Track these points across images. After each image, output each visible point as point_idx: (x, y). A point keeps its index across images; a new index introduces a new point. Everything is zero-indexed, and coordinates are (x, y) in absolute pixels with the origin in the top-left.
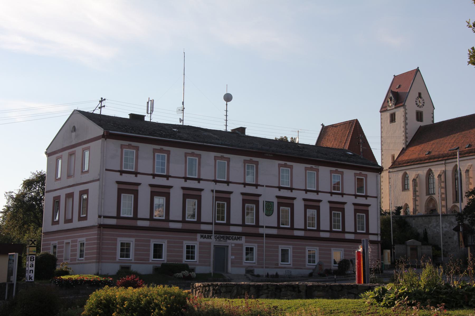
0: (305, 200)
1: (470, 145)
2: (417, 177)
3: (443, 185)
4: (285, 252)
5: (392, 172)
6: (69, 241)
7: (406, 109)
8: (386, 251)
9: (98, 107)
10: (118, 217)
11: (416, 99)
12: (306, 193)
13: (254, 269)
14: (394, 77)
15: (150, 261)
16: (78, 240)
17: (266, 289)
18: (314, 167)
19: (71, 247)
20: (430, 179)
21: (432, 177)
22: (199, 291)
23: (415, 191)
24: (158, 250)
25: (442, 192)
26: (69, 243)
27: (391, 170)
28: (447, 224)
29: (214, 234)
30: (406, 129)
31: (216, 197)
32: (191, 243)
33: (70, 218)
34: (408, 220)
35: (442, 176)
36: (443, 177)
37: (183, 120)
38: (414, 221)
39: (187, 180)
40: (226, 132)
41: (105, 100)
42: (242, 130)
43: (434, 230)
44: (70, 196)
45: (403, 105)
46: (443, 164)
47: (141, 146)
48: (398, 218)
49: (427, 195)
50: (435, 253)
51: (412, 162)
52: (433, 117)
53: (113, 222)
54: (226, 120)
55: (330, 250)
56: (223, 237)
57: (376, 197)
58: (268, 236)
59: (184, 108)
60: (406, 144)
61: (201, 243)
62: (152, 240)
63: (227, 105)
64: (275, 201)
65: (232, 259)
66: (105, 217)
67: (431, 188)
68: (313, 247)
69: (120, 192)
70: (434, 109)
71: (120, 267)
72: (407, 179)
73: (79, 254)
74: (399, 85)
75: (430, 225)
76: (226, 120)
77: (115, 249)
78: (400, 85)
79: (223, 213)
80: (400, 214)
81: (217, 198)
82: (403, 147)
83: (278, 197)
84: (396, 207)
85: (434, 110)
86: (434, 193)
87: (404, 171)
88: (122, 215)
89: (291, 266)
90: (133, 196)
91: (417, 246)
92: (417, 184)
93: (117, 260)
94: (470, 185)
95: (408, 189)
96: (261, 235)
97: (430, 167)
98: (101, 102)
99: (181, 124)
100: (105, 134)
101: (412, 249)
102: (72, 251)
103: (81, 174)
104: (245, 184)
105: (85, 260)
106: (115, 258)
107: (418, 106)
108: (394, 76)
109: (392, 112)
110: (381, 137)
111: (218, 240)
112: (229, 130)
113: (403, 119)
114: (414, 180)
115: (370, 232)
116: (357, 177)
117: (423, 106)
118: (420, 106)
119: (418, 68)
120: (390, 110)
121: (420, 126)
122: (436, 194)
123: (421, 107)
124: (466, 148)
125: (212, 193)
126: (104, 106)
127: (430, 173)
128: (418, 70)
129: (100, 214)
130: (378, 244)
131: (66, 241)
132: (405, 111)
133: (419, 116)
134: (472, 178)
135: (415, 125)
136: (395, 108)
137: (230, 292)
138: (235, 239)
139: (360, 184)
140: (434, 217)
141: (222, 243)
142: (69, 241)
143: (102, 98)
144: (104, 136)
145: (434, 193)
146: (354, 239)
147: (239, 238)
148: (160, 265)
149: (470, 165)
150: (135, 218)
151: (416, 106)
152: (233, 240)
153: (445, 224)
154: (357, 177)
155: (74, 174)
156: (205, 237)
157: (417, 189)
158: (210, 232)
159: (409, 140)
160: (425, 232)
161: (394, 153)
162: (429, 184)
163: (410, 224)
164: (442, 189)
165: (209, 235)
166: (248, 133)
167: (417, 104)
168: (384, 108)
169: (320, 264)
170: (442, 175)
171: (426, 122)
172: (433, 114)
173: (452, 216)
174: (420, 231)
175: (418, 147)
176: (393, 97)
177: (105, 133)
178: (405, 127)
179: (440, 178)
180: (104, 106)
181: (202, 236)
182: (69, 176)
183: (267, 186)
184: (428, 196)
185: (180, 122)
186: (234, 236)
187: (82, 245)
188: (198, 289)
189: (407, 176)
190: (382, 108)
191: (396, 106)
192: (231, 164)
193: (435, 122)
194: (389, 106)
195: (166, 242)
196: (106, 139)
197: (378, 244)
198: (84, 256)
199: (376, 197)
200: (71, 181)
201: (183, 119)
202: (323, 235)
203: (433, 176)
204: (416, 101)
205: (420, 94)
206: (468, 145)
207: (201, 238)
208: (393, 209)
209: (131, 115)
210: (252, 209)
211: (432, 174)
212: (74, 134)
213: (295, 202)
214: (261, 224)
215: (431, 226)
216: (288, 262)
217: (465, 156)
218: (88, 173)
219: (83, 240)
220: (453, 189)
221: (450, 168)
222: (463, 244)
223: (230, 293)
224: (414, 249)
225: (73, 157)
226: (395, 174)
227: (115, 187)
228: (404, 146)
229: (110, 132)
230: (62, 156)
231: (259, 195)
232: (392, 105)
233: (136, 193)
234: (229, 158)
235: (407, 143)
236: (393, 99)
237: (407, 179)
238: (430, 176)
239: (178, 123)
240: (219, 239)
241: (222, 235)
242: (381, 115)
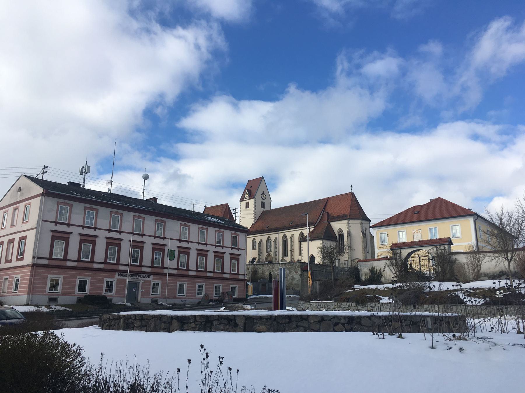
0: (197, 250)
4: (181, 287)
6: (7, 277)
9: (41, 172)
10: (50, 258)
12: (198, 245)
13: (158, 299)
15: (75, 294)
16: (15, 277)
17: (193, 322)
18: (205, 227)
19: (8, 282)
21: (270, 242)
22: (107, 324)
23: (260, 250)
24: (82, 286)
25: (276, 250)
26: (7, 279)
29: (129, 273)
30: (255, 212)
31: (132, 245)
32: (110, 280)
33: (10, 258)
37: (111, 190)
39: (111, 232)
40: (143, 200)
41: (47, 167)
42: (155, 199)
44: (11, 241)
47: (75, 204)
49: (266, 252)
52: (270, 206)
53: (46, 262)
54: (144, 193)
56: (136, 276)
57: (245, 250)
58: (171, 275)
59: (112, 182)
61: (118, 280)
62: (78, 277)
63: (144, 182)
64: (177, 250)
65: (142, 292)
66: (38, 258)
68: (201, 283)
69: (53, 238)
71: (48, 298)
73: (14, 288)
76: (144, 193)
77: (46, 284)
79: (137, 257)
81: (133, 247)
83: (178, 247)
85: (271, 202)
87: (254, 238)
88: (54, 257)
89: (185, 297)
90: (64, 242)
93: (47, 293)
95: (256, 249)
96: (165, 274)
97: (270, 236)
98: (44, 169)
99: (110, 192)
100: (44, 193)
102: (9, 285)
103: (22, 224)
104: (155, 237)
105: (18, 293)
106: (45, 291)
107: (262, 199)
111: (132, 277)
112: (145, 199)
113: (253, 206)
115: (240, 273)
116: (233, 235)
125: (130, 242)
126: (46, 172)
127: (269, 239)
129: (34, 256)
130: (244, 281)
131: (5, 277)
133: (263, 205)
135: (260, 210)
136: (249, 199)
137: (146, 326)
138: (145, 277)
139: (234, 240)
140: (276, 265)
141: (135, 280)
142: (7, 277)
143: (45, 166)
144: (42, 194)
147: (148, 276)
148: (83, 297)
150: (65, 259)
152: (143, 277)
154: (233, 235)
155: (16, 224)
156: (122, 275)
158: (126, 271)
165: (125, 273)
166: (158, 202)
167: (262, 198)
169: (206, 295)
171: (267, 208)
172: (271, 204)
177: (44, 191)
180: (46, 172)
181: (119, 275)
182: (12, 225)
183: (171, 239)
185: (109, 191)
186: (145, 275)
187: (17, 280)
188: (106, 321)
189: (255, 241)
192: (146, 222)
193: (272, 209)
195: (90, 279)
196: (45, 197)
198: (18, 290)
199: (245, 250)
200: (14, 230)
201: (111, 189)
202: (209, 275)
204: (261, 196)
205: (263, 192)
207: (118, 276)
209: (70, 183)
210: (159, 255)
212: (19, 193)
213: (191, 251)
214: (165, 266)
216: (183, 294)
218: (28, 223)
219: (18, 276)
221: (281, 235)
222: (311, 279)
223: (145, 328)
225: (17, 211)
227: (49, 235)
229: (49, 191)
230: (8, 210)
231: (165, 245)
233: (67, 240)
234: (145, 217)
235: (256, 221)
239: (107, 191)
240: (133, 277)
241: (135, 274)
242: (240, 203)
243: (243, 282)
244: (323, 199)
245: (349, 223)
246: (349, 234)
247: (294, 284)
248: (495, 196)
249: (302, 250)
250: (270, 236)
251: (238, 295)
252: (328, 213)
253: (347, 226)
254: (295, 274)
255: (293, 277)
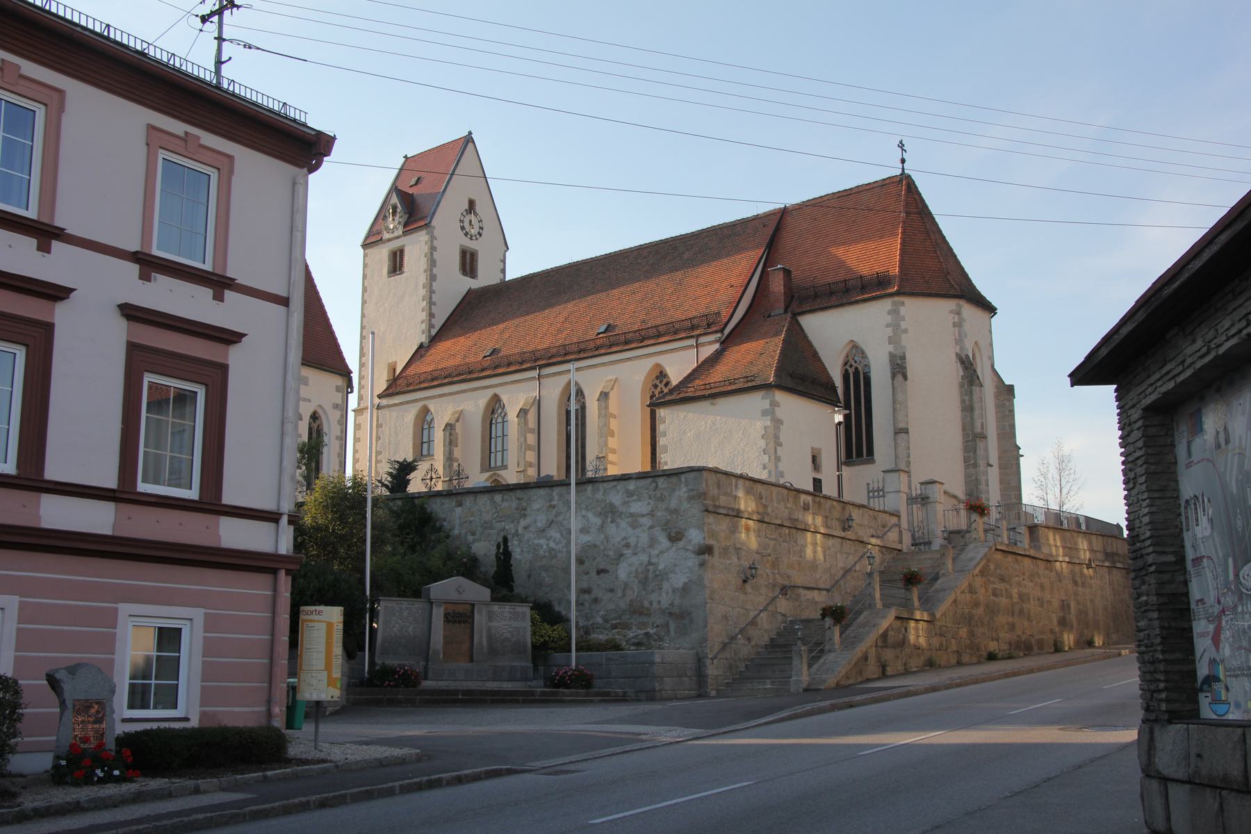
1: (609, 326)
2: (457, 420)
3: (531, 439)
5: (388, 406)
7: (433, 238)
8: (320, 613)
11: (462, 214)
14: (404, 159)
20: (493, 426)
21: (500, 420)
27: (384, 402)
28: (590, 515)
30: (431, 292)
34: (435, 507)
35: (530, 412)
36: (532, 416)
38: (459, 510)
43: (536, 542)
45: (426, 224)
46: (533, 378)
48: (399, 503)
49: (483, 470)
50: (542, 636)
51: (445, 378)
55: (111, 619)
60: (430, 332)
67: (496, 452)
70: (506, 249)
72: (429, 426)
74: (416, 179)
75: (523, 523)
78: (419, 179)
80: (405, 491)
82: (420, 342)
84: (390, 462)
86: (505, 464)
87: (421, 404)
91: (473, 605)
92: (457, 439)
94: (609, 438)
97: (497, 391)
101: (450, 618)
107: (466, 234)
108: (406, 157)
109: (395, 245)
110: (363, 316)
113: (423, 263)
114: (449, 427)
117: (478, 236)
118: (472, 236)
119: (470, 133)
120: (389, 240)
121: (470, 292)
122: (509, 467)
123: (474, 238)
124: (599, 334)
127: (495, 407)
128: (469, 140)
130: (274, 572)
132: (432, 241)
133: (469, 263)
134: (615, 417)
135: (457, 286)
136: (405, 233)
140: (542, 492)
145: (505, 464)
146: (108, 531)
149: (610, 380)
151: (462, 234)
153: (584, 517)
157: (457, 453)
159: (439, 322)
160: (501, 551)
161: (394, 360)
162: (491, 438)
163: (445, 524)
164: (527, 452)
167: (463, 228)
168: (373, 235)
170: (531, 410)
171: (486, 278)
172: (504, 261)
173: (615, 483)
174: (484, 549)
175: (462, 339)
176: (399, 205)
178: (429, 285)
179: (523, 420)
184: (487, 474)
189: (429, 418)
190: (367, 237)
191: (406, 230)
194: (387, 229)
197: (274, 572)
203: (503, 414)
204: (461, 221)
205: (472, 204)
206: (605, 327)
208: (384, 470)
211: (500, 411)
215: (526, 528)
217: (596, 353)
220: (559, 453)
224: (460, 617)
226: (394, 414)
228: (424, 339)
232: (395, 227)
235: (434, 332)
236: (398, 210)
237: (429, 426)
238: (496, 416)
242: (365, 256)
243: (265, 579)
244: (756, 218)
245: (894, 312)
246: (899, 368)
247: (663, 611)
248: (1015, 443)
249: (665, 447)
250: (497, 391)
251: (207, 696)
252: (787, 273)
253: (890, 329)
254: (664, 542)
255: (650, 563)
